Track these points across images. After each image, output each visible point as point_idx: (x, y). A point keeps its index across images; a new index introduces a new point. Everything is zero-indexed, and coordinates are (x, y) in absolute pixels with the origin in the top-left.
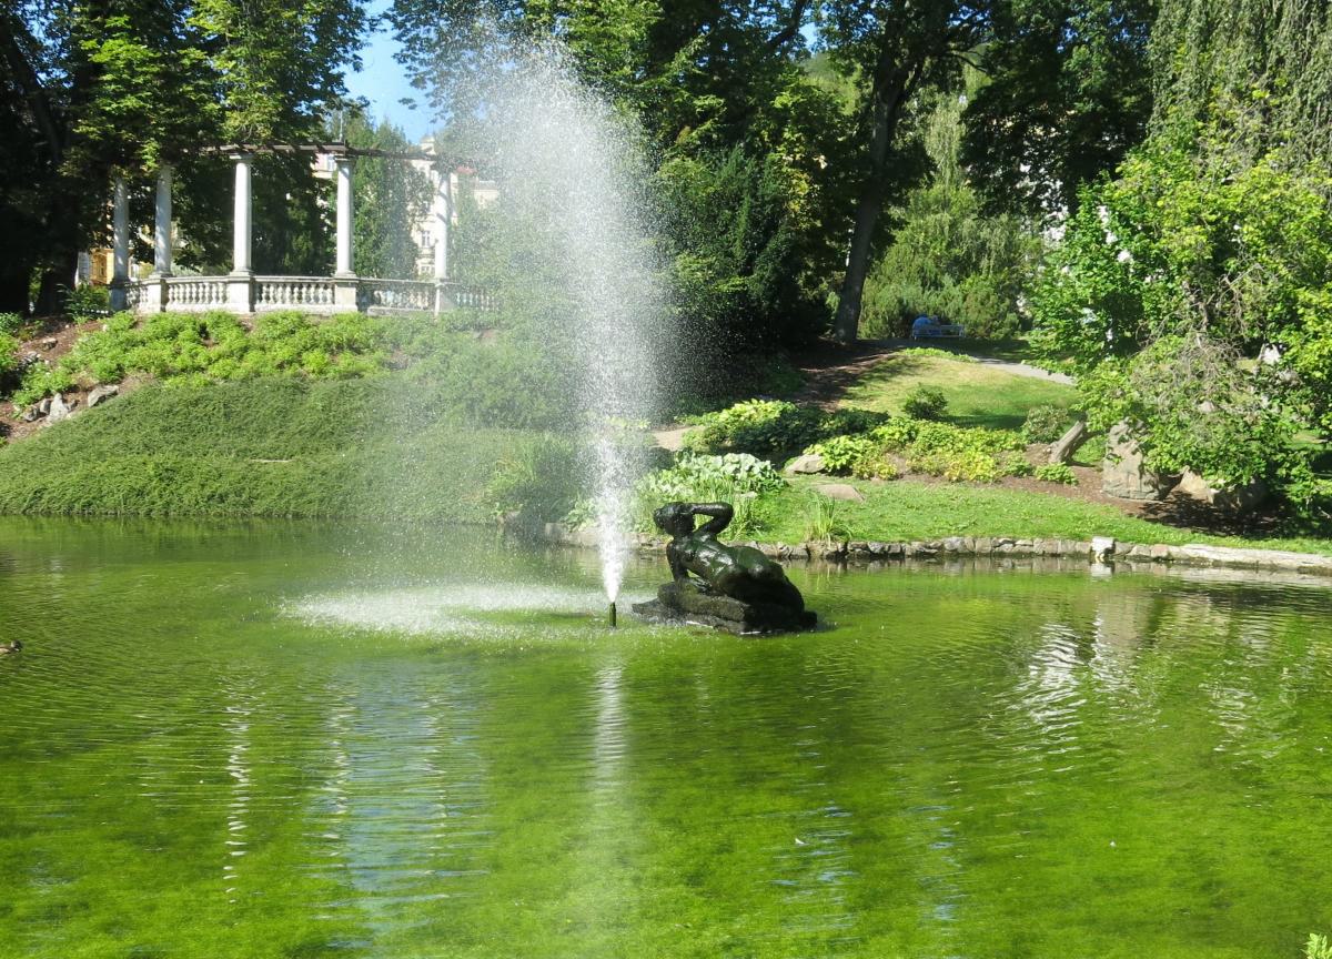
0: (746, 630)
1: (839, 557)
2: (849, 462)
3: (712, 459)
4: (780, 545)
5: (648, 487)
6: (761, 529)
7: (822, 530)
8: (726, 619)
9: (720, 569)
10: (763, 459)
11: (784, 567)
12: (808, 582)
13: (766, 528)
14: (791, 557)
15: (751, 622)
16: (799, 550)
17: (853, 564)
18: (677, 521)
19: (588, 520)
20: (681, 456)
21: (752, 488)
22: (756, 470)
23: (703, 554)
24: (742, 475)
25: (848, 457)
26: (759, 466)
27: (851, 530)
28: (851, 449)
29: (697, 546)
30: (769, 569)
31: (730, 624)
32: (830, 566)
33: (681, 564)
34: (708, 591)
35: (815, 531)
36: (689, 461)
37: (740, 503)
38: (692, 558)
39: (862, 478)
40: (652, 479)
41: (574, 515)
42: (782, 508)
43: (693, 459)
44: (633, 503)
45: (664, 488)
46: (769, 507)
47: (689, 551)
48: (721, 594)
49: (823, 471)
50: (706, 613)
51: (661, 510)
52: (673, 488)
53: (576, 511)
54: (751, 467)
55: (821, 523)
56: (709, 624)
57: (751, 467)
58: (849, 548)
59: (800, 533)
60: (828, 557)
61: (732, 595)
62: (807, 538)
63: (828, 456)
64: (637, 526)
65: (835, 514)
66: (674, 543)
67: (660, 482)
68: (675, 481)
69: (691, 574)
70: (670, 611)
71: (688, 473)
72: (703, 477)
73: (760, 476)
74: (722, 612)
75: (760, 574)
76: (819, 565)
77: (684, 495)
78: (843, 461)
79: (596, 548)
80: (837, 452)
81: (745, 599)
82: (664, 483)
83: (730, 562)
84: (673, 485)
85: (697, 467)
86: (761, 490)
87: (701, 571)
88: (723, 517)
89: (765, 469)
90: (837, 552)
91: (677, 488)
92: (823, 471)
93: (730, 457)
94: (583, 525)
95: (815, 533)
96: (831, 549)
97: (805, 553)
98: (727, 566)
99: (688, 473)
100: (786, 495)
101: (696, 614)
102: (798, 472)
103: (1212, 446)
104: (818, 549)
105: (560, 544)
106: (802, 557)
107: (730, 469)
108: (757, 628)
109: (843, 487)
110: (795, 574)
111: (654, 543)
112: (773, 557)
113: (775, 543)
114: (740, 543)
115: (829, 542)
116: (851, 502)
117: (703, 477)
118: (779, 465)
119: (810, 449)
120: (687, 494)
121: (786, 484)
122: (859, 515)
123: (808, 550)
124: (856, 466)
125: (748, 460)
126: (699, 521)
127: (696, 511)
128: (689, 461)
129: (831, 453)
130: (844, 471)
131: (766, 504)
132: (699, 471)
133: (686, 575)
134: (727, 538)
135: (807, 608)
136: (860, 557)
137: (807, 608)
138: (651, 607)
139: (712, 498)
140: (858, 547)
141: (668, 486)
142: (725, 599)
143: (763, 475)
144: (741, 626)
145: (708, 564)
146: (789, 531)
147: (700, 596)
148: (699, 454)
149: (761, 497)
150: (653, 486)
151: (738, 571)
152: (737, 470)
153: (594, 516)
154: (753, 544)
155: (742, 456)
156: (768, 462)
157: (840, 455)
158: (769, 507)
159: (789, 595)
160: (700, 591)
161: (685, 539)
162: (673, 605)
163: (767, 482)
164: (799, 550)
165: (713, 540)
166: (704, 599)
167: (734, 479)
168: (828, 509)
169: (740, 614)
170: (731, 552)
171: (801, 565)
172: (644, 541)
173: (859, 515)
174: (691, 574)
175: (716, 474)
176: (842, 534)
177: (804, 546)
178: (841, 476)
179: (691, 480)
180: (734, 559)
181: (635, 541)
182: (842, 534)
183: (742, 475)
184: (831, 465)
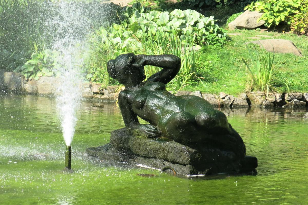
0: (191, 173)
1: (277, 107)
2: (287, 19)
3: (159, 14)
4: (222, 95)
5: (100, 39)
6: (205, 80)
7: (262, 82)
8: (174, 162)
9: (168, 116)
10: (207, 15)
11: (226, 114)
12: (254, 132)
13: (209, 80)
14: (232, 106)
15: (197, 166)
16: (240, 99)
17: (289, 113)
18: (129, 71)
19: (44, 70)
20: (130, 11)
21: (197, 42)
22: (201, 26)
23: (152, 103)
24: (188, 30)
25: (286, 14)
26: (204, 21)
27: (288, 81)
28: (289, 6)
29: (145, 93)
30: (213, 117)
31: (177, 167)
32: (269, 114)
33: (131, 111)
34: (157, 136)
35: (256, 82)
36: (138, 16)
37: (187, 54)
38: (142, 105)
39: (299, 33)
40: (104, 32)
41: (31, 65)
42: (224, 61)
43: (142, 14)
44: (86, 55)
45: (115, 41)
46: (212, 60)
47: (140, 99)
48: (170, 139)
49: (262, 27)
50: (155, 158)
51: (114, 61)
52: (124, 42)
53: (32, 61)
54: (196, 23)
55: (260, 74)
56: (156, 166)
57: (196, 23)
58: (286, 97)
59: (241, 84)
60: (267, 107)
61: (180, 141)
62: (247, 88)
63: (268, 13)
64: (89, 76)
65: (274, 66)
66: (126, 91)
67: (111, 35)
68: (126, 34)
69: (142, 121)
70: (120, 155)
71: (137, 28)
72: (153, 31)
73: (204, 31)
74: (170, 156)
75: (204, 121)
76: (257, 114)
77: (133, 49)
78: (282, 17)
79: (51, 96)
80: (276, 9)
81: (190, 145)
82: (115, 37)
83: (178, 110)
84: (123, 38)
85: (145, 22)
86: (205, 43)
87: (151, 119)
88: (171, 69)
89: (209, 25)
90: (275, 102)
91: (126, 42)
92: (262, 27)
93: (176, 12)
94: (39, 74)
95: (255, 84)
96: (271, 99)
97: (245, 103)
98: (175, 114)
99: (137, 28)
100: (227, 49)
101: (145, 157)
102: (240, 28)
103: (186, 94)
104: (258, 99)
105: (20, 92)
106: (243, 107)
107: (176, 24)
108: (202, 171)
109: (282, 42)
110: (236, 121)
111: (106, 92)
112: (216, 106)
113: (217, 93)
114: (185, 93)
115: (268, 93)
116: (288, 55)
117: (153, 31)
118: (221, 21)
119: (251, 6)
120: (138, 48)
121: (228, 39)
122: (296, 68)
123: (248, 100)
124: (294, 22)
125: (193, 15)
126: (150, 71)
127: (145, 63)
128: (138, 16)
129: (271, 10)
130: (283, 27)
131: (210, 57)
132: (147, 26)
133: (137, 121)
134: (173, 87)
135: (249, 153)
136: (297, 107)
137: (249, 153)
138: (103, 151)
139: (159, 51)
140: (295, 97)
141: (118, 39)
142: (174, 144)
143: (207, 30)
144: (187, 169)
145: (158, 112)
146: (231, 82)
147: (151, 141)
148: (146, 10)
149: (205, 51)
150: (104, 39)
151: (186, 118)
152: (183, 25)
153: (48, 65)
154: (197, 94)
155: (188, 12)
156: (211, 18)
157: (279, 12)
158: (212, 60)
159: (234, 141)
160: (150, 137)
161: (136, 88)
162: (124, 150)
163: (210, 37)
164: (240, 99)
165: (162, 89)
166: (154, 144)
167: (180, 33)
168: (269, 64)
169: (186, 158)
170: (179, 100)
171: (241, 114)
172: (96, 89)
173: (296, 68)
174: (142, 121)
175: (161, 29)
176: (280, 85)
177: (244, 96)
178: (280, 31)
179: (140, 33)
180: (181, 109)
181: (88, 90)
182: (280, 85)
183: (188, 30)
184: (270, 21)
